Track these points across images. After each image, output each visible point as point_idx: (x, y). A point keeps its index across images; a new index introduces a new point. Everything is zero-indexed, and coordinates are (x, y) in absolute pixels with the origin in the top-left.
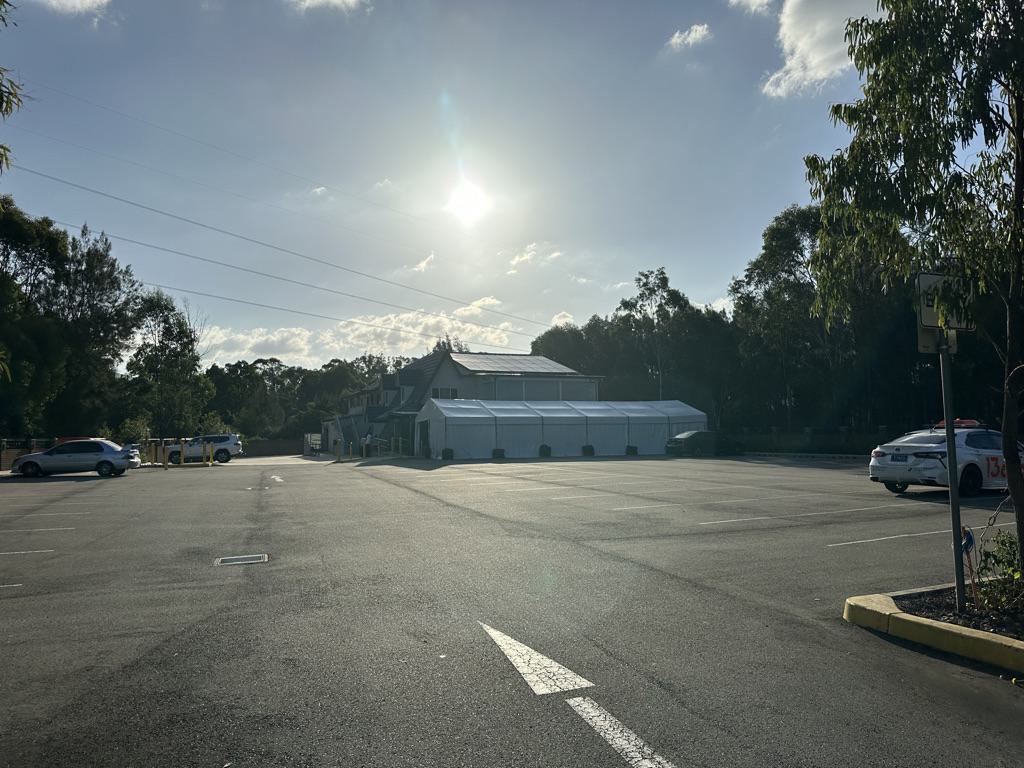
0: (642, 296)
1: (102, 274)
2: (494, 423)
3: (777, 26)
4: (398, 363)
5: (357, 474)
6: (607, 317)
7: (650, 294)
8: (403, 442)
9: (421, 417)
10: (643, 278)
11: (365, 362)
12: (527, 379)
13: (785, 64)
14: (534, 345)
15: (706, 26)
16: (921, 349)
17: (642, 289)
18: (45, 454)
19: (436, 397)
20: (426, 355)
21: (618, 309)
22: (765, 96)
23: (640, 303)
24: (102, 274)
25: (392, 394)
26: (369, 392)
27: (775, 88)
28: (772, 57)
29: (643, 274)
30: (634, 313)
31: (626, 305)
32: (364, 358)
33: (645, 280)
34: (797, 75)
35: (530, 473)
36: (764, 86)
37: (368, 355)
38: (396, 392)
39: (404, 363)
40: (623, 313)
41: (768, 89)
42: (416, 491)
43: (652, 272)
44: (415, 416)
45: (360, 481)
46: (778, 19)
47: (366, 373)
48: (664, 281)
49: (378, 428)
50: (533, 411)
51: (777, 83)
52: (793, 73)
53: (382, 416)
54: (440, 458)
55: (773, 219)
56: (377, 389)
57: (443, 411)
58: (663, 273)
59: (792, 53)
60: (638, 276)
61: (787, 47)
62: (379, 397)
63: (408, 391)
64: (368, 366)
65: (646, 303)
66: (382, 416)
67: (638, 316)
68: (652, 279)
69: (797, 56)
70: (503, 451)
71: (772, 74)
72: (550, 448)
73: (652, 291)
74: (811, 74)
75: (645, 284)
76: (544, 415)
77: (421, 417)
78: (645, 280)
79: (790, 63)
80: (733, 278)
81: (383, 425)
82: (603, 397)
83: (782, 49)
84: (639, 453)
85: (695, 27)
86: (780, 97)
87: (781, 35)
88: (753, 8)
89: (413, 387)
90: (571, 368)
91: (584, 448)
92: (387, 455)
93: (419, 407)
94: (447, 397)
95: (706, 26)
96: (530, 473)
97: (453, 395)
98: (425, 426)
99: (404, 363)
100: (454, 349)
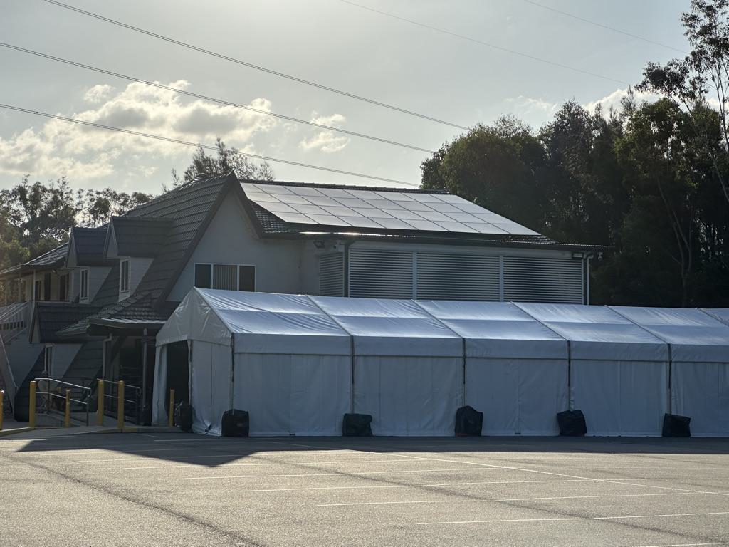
0: (697, 57)
2: (348, 351)
4: (101, 207)
5: (23, 470)
6: (599, 108)
7: (717, 54)
8: (127, 391)
9: (172, 330)
10: (701, 15)
11: (24, 200)
12: (421, 248)
14: (431, 169)
18: (26, 449)
19: (205, 285)
20: (171, 188)
21: (641, 87)
23: (693, 74)
25: (97, 276)
26: (40, 269)
30: (676, 99)
31: (658, 77)
32: (21, 191)
35: (457, 478)
37: (31, 183)
38: (107, 271)
39: (114, 207)
40: (653, 96)
42: (188, 519)
44: (155, 330)
45: (37, 488)
47: (25, 226)
49: (62, 356)
50: (441, 325)
53: (74, 328)
54: (217, 431)
56: (61, 263)
57: (227, 319)
60: (690, 11)
62: (64, 282)
63: (137, 269)
64: (31, 211)
65: (707, 74)
66: (74, 328)
67: (686, 107)
70: (368, 419)
72: (247, 413)
75: (707, 30)
76: (468, 335)
77: (172, 330)
78: (706, 21)
81: (73, 350)
82: (600, 296)
89: (150, 261)
90: (538, 232)
91: (560, 417)
92: (87, 422)
93: (166, 309)
94: (231, 287)
96: (457, 478)
97: (246, 282)
98: (179, 354)
99: (114, 207)
100: (687, 84)
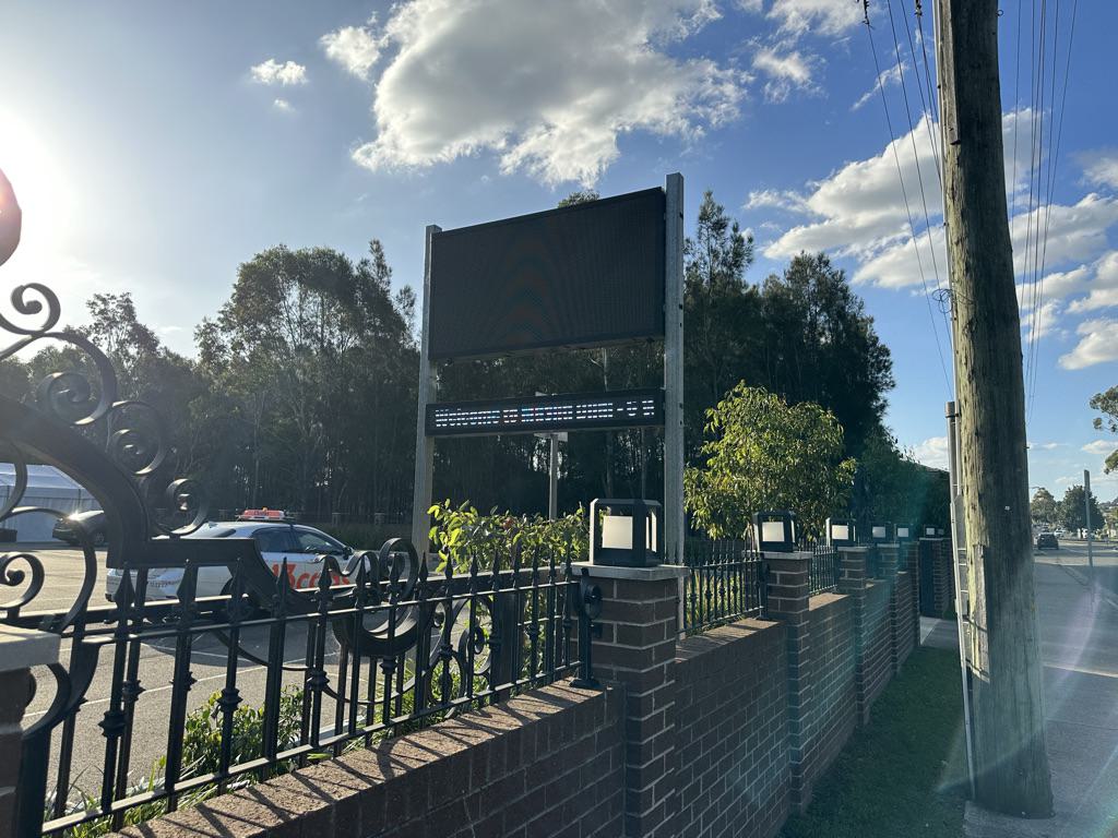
1: (334, 305)
3: (373, 97)
10: (99, 303)
13: (377, 137)
15: (303, 68)
16: (151, 572)
17: (99, 317)
22: (354, 163)
24: (334, 305)
27: (365, 157)
28: (367, 129)
29: (98, 297)
33: (102, 307)
34: (388, 152)
36: (354, 151)
41: (357, 155)
43: (113, 297)
46: (374, 89)
48: (129, 311)
51: (368, 154)
52: (384, 148)
55: (254, 257)
58: (128, 300)
59: (385, 128)
60: (92, 299)
61: (380, 120)
68: (112, 306)
69: (389, 133)
71: (365, 143)
73: (113, 323)
74: (402, 155)
75: (102, 312)
78: (102, 307)
79: (383, 138)
80: (205, 320)
83: (375, 121)
84: (18, 540)
85: (291, 64)
86: (369, 170)
87: (376, 107)
88: (352, 68)
95: (303, 68)
